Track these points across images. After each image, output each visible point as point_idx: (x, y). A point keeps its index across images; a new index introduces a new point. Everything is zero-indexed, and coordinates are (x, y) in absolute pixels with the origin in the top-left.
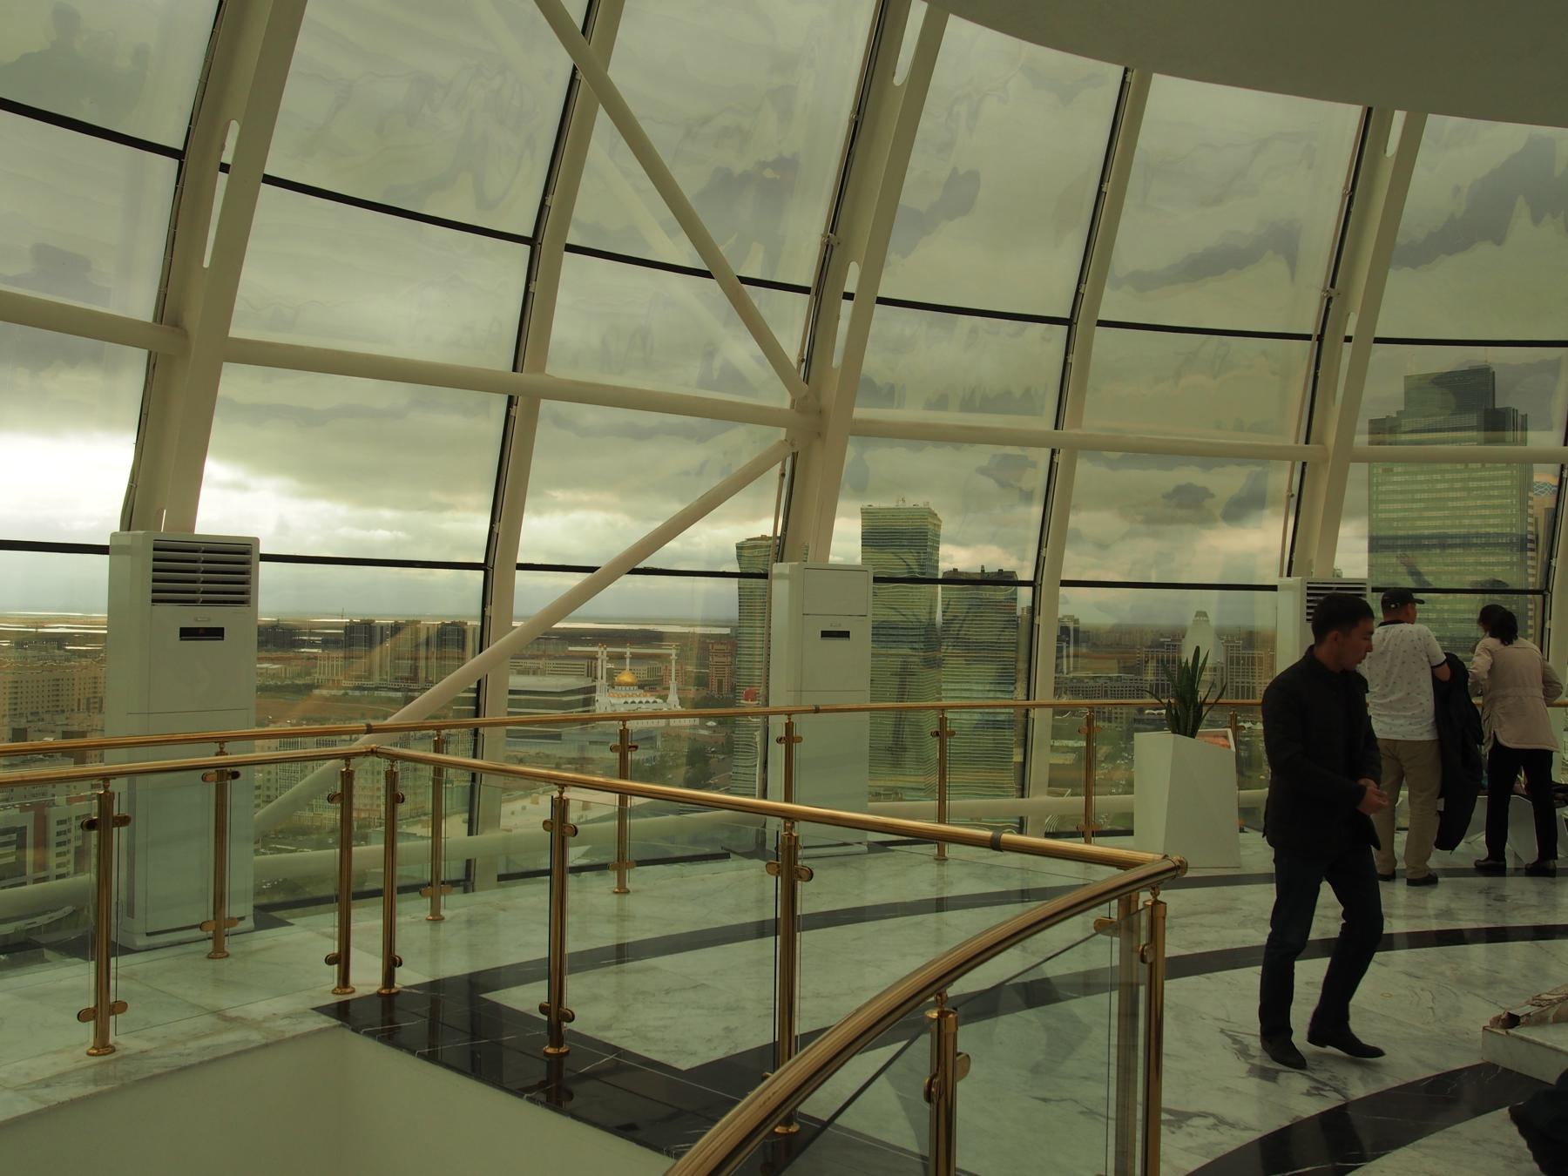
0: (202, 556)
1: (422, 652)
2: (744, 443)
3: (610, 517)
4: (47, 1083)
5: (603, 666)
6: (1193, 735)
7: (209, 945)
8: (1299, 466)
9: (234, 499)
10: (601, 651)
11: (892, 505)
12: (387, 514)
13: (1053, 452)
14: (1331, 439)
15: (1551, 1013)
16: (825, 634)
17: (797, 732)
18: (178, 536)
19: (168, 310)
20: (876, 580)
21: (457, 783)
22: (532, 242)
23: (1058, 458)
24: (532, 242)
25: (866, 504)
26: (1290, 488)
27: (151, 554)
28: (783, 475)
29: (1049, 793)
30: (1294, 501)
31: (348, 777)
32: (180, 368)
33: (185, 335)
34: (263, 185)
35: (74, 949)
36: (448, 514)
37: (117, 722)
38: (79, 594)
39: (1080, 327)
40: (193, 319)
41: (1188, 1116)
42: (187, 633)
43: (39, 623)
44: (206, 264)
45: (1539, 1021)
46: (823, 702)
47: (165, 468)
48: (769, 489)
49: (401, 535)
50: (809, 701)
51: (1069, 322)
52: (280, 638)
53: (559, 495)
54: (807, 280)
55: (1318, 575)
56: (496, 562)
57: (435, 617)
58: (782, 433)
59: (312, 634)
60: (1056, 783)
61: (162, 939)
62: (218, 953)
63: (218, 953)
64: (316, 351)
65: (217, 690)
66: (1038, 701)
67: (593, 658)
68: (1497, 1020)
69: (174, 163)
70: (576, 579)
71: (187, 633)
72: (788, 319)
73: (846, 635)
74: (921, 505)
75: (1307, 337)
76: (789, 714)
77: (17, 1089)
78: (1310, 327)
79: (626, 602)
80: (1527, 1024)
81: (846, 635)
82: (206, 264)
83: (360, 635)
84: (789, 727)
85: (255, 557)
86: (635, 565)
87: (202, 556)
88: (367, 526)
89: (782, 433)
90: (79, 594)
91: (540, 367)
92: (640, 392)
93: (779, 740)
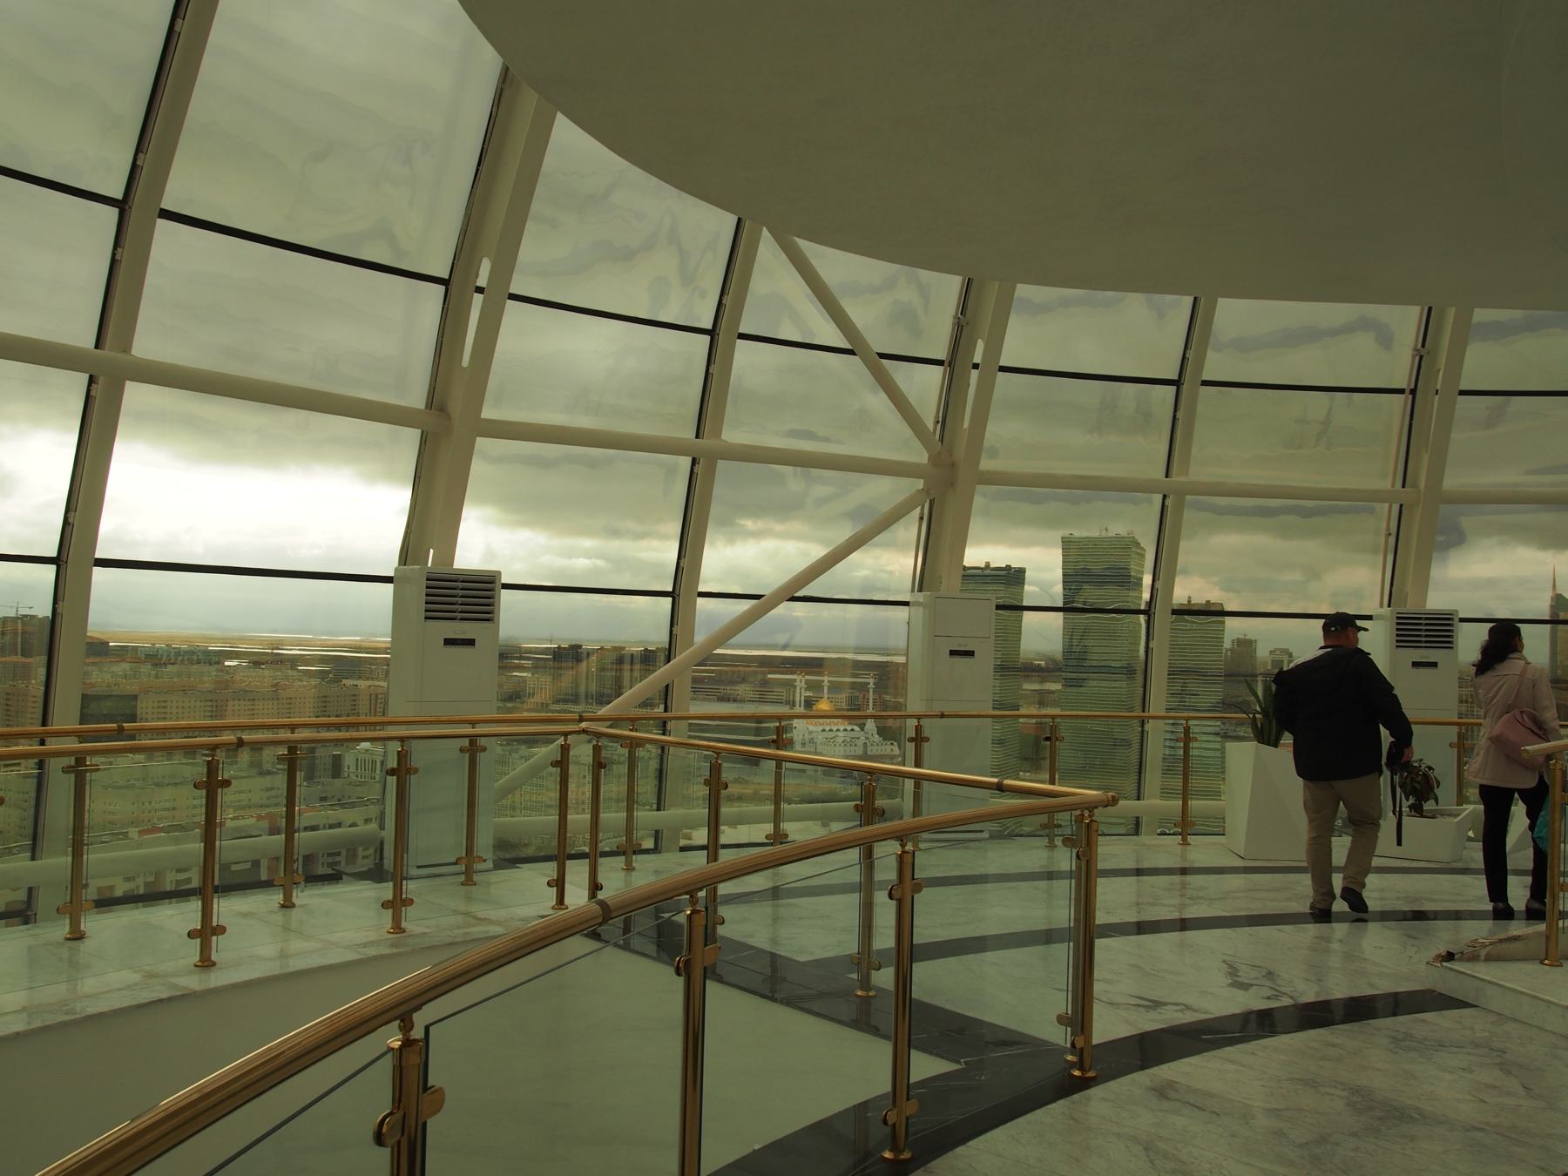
0: (460, 585)
1: (627, 667)
2: (883, 491)
3: (802, 545)
4: (365, 945)
5: (801, 694)
6: (1276, 745)
7: (463, 878)
8: (1396, 508)
9: (483, 541)
10: (800, 680)
11: (1095, 534)
12: (587, 543)
13: (1165, 497)
14: (1422, 484)
15: (1483, 952)
16: (953, 653)
17: (926, 733)
18: (443, 570)
19: (436, 400)
20: (999, 607)
21: (648, 754)
22: (712, 333)
23: (1168, 502)
24: (712, 333)
25: (1066, 533)
26: (1388, 529)
27: (425, 583)
28: (922, 518)
29: (1162, 798)
30: (1392, 540)
31: (565, 749)
32: (443, 437)
33: (449, 417)
34: (509, 302)
35: (376, 874)
36: (644, 543)
37: (397, 710)
38: (367, 617)
39: (1185, 388)
40: (456, 406)
41: (1166, 1004)
42: (449, 642)
43: (278, 644)
44: (466, 362)
45: (1473, 958)
46: (948, 710)
47: (432, 517)
48: (909, 531)
49: (600, 563)
50: (937, 708)
51: (1176, 383)
52: (508, 656)
53: (749, 524)
54: (941, 354)
55: (1410, 607)
56: (682, 587)
57: (637, 643)
58: (920, 484)
59: (521, 658)
60: (1166, 793)
61: (433, 870)
62: (469, 882)
63: (469, 882)
64: (544, 427)
65: (465, 687)
66: (1152, 713)
67: (791, 685)
68: (1438, 956)
69: (443, 288)
70: (746, 605)
71: (449, 642)
72: (924, 385)
73: (970, 654)
74: (1123, 533)
75: (1401, 391)
76: (919, 717)
77: (347, 947)
78: (1401, 381)
79: (803, 628)
80: (1461, 960)
81: (970, 654)
82: (466, 362)
83: (569, 655)
84: (918, 729)
85: (498, 586)
86: (792, 593)
87: (460, 585)
88: (571, 553)
89: (920, 484)
90: (367, 617)
91: (718, 434)
92: (797, 452)
93: (911, 740)
